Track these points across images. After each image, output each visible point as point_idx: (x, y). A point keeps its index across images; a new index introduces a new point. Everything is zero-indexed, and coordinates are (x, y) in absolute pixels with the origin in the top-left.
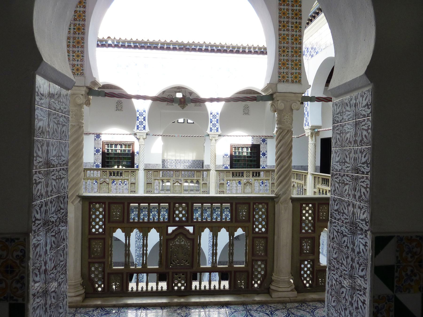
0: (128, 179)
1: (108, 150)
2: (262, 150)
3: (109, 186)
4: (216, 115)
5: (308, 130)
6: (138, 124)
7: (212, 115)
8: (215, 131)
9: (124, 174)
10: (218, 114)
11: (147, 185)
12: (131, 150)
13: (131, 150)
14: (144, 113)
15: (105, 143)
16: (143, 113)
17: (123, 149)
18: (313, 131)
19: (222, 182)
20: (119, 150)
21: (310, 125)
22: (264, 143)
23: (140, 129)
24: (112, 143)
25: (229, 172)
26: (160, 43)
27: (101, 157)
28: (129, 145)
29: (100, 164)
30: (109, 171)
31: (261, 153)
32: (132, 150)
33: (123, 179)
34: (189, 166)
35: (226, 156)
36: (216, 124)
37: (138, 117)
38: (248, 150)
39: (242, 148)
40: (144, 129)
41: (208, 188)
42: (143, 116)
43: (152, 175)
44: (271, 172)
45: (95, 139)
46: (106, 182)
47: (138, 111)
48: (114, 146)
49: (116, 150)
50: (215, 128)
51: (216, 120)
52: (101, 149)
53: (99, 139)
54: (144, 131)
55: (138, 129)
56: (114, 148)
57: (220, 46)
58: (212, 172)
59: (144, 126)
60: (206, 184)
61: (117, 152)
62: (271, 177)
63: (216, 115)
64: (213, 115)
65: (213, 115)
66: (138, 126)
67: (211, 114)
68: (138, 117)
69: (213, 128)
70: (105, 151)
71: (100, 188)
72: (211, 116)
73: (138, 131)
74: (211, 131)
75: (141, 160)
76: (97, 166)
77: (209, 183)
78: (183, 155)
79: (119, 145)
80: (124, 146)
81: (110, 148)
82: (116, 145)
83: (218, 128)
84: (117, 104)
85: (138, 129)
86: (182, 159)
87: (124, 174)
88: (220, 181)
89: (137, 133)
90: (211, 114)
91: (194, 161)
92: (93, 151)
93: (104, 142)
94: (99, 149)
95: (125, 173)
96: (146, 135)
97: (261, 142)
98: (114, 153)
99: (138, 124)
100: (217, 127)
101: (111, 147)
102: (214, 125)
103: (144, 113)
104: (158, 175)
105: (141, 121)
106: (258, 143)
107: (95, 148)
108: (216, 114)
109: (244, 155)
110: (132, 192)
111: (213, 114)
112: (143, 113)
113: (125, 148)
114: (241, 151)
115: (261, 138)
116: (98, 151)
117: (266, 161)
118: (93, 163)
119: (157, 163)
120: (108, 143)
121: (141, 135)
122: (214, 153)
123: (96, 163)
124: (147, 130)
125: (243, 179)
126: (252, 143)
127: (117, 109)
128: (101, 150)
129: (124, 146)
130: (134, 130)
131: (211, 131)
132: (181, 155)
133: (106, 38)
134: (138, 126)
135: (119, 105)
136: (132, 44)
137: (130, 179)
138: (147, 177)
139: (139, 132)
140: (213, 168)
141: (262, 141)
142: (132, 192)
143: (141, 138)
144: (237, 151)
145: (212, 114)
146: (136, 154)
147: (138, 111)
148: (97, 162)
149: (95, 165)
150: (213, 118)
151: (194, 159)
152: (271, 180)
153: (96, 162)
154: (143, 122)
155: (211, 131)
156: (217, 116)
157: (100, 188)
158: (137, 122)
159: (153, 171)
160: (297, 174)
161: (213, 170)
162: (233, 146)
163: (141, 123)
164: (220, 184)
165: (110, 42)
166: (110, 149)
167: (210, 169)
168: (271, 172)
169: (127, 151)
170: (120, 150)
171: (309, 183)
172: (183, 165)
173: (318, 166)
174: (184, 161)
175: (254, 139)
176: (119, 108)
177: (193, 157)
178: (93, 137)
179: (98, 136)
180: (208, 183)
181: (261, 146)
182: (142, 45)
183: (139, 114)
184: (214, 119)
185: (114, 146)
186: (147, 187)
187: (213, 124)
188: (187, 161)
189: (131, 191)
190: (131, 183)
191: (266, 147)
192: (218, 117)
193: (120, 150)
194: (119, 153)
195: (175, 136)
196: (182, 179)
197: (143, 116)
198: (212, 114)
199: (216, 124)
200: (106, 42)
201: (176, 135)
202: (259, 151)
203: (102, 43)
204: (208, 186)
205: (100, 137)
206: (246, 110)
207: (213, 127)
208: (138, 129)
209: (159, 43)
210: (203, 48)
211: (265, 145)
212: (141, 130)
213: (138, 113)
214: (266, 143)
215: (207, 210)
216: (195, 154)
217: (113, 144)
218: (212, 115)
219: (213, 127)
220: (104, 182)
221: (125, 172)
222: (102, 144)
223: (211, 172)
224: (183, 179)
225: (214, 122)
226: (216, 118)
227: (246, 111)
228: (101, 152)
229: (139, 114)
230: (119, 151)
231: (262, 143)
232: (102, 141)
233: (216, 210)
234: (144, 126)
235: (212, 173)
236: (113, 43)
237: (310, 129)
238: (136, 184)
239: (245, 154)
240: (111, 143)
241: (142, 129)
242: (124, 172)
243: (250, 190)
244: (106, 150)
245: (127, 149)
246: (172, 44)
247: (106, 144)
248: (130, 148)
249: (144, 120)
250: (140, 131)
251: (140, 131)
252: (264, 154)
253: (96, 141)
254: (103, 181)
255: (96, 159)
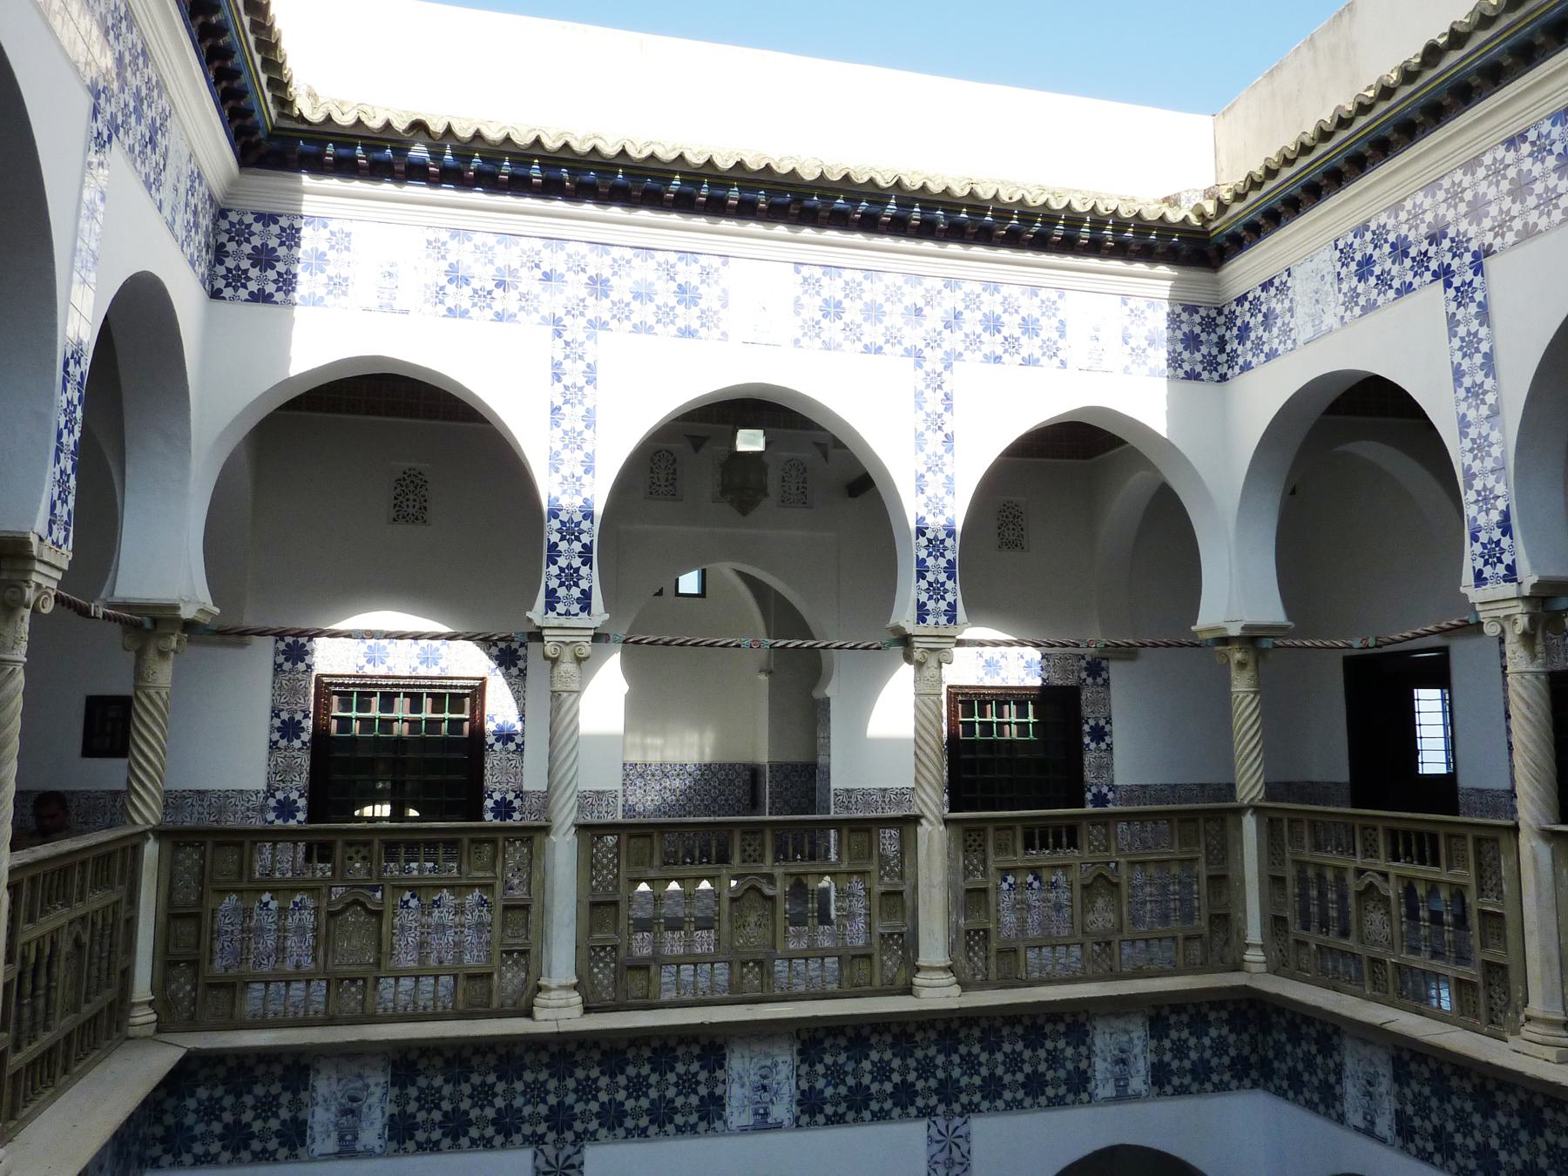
0: (492, 885)
1: (345, 723)
2: (1090, 716)
3: (384, 929)
4: (942, 541)
5: (1514, 603)
6: (554, 583)
7: (923, 541)
8: (943, 620)
9: (469, 856)
10: (951, 533)
11: (591, 913)
12: (467, 725)
13: (467, 725)
14: (585, 525)
15: (331, 684)
16: (578, 524)
17: (423, 715)
18: (1540, 611)
19: (977, 880)
20: (404, 721)
21: (1528, 578)
22: (1094, 679)
23: (561, 608)
24: (370, 686)
25: (1011, 828)
26: (681, 173)
27: (305, 760)
28: (457, 701)
29: (300, 796)
30: (382, 841)
31: (1086, 728)
32: (472, 720)
33: (464, 881)
34: (683, 793)
35: (505, 744)
36: (943, 584)
37: (556, 545)
38: (1027, 716)
39: (1000, 705)
40: (586, 606)
41: (908, 913)
42: (578, 539)
43: (617, 855)
44: (1201, 821)
45: (280, 665)
46: (363, 905)
47: (556, 516)
48: (375, 701)
49: (387, 724)
50: (943, 605)
51: (942, 562)
52: (306, 716)
53: (301, 666)
54: (583, 620)
55: (550, 606)
56: (375, 712)
57: (968, 206)
58: (930, 828)
59: (583, 591)
60: (901, 893)
61: (391, 732)
62: (1203, 846)
63: (942, 541)
64: (930, 541)
65: (930, 541)
66: (551, 593)
67: (921, 532)
68: (556, 545)
69: (931, 605)
70: (328, 730)
71: (327, 942)
72: (918, 547)
73: (552, 619)
74: (921, 618)
75: (560, 775)
76: (286, 809)
77: (915, 888)
78: (659, 741)
79: (406, 695)
80: (427, 703)
81: (354, 714)
82: (388, 701)
83: (952, 606)
84: (398, 491)
85: (553, 609)
86: (654, 758)
87: (469, 856)
88: (966, 877)
89: (546, 632)
90: (921, 532)
91: (708, 771)
92: (260, 730)
93: (326, 680)
94: (299, 716)
95: (472, 851)
96: (589, 639)
97: (1084, 675)
98: (376, 738)
99: (554, 583)
100: (949, 597)
101: (364, 706)
102: (936, 590)
103: (585, 525)
104: (652, 856)
105: (570, 566)
106: (1072, 681)
107: (278, 716)
108: (942, 535)
109: (1007, 737)
110: (510, 953)
111: (930, 534)
112: (578, 524)
113: (433, 711)
114: (995, 719)
115: (1083, 658)
116: (289, 729)
117: (1109, 767)
118: (261, 795)
119: (600, 788)
120: (348, 685)
121: (568, 640)
122: (931, 729)
123: (280, 795)
124: (599, 614)
125: (1078, 862)
126: (1044, 680)
127: (401, 515)
128: (309, 724)
129: (430, 700)
130: (529, 614)
131: (924, 621)
132: (649, 741)
133: (400, 125)
134: (554, 591)
135: (411, 497)
136: (535, 172)
137: (499, 885)
138: (589, 864)
139: (555, 623)
140: (933, 807)
141: (1086, 669)
142: (510, 953)
143: (567, 655)
144: (977, 719)
145: (924, 534)
146: (490, 740)
147: (556, 516)
148: (282, 785)
149: (272, 802)
150: (930, 554)
151: (707, 759)
152: (1203, 860)
153: (278, 789)
154: (577, 570)
155: (924, 621)
156: (949, 542)
157: (327, 942)
158: (548, 575)
159: (624, 838)
160: (1313, 824)
161: (932, 819)
162: (960, 698)
163: (570, 577)
164: (968, 891)
165: (419, 152)
166: (357, 719)
167: (917, 811)
168: (1201, 821)
169: (445, 726)
170: (406, 724)
171: (1538, 883)
172: (658, 788)
173: (1337, 784)
174: (664, 771)
175: (1051, 664)
176: (411, 510)
177: (702, 753)
178: (264, 653)
179: (296, 652)
180: (906, 888)
181: (1086, 695)
182: (586, 178)
183: (559, 531)
184: (936, 558)
185: (375, 701)
186: (591, 926)
187: (930, 584)
188: (677, 768)
189: (505, 952)
190: (506, 908)
191: (1106, 703)
192: (953, 551)
193: (406, 724)
194: (400, 739)
195: (738, 646)
196: (778, 871)
197: (578, 539)
198: (924, 534)
199: (943, 584)
200: (401, 146)
201: (746, 642)
202: (1078, 720)
203: (376, 155)
204: (909, 903)
205: (307, 653)
206: (1011, 527)
207: (930, 598)
208: (553, 609)
209: (675, 173)
210: (888, 212)
211: (1099, 689)
212: (568, 613)
213: (555, 524)
214: (1106, 683)
215: (918, 1038)
216: (710, 738)
217: (374, 694)
218: (923, 541)
219: (930, 598)
220: (356, 902)
221: (473, 846)
222: (313, 691)
223: (924, 829)
224: (782, 870)
225: (937, 573)
226: (943, 555)
227: (1011, 532)
228: (306, 737)
229: (559, 531)
230: (400, 729)
231: (1090, 681)
232: (314, 674)
233: (962, 1035)
234: (583, 591)
235: (930, 839)
236: (437, 155)
237: (1524, 598)
238: (533, 909)
239: (1012, 733)
240: (365, 685)
241: (575, 608)
242: (466, 842)
243: (1112, 916)
244: (334, 723)
245: (447, 715)
246: (737, 179)
247: (335, 693)
248: (462, 712)
249: (587, 561)
250: (564, 621)
251: (564, 621)
252: (1099, 734)
253: (284, 679)
254: (350, 899)
255: (278, 774)
